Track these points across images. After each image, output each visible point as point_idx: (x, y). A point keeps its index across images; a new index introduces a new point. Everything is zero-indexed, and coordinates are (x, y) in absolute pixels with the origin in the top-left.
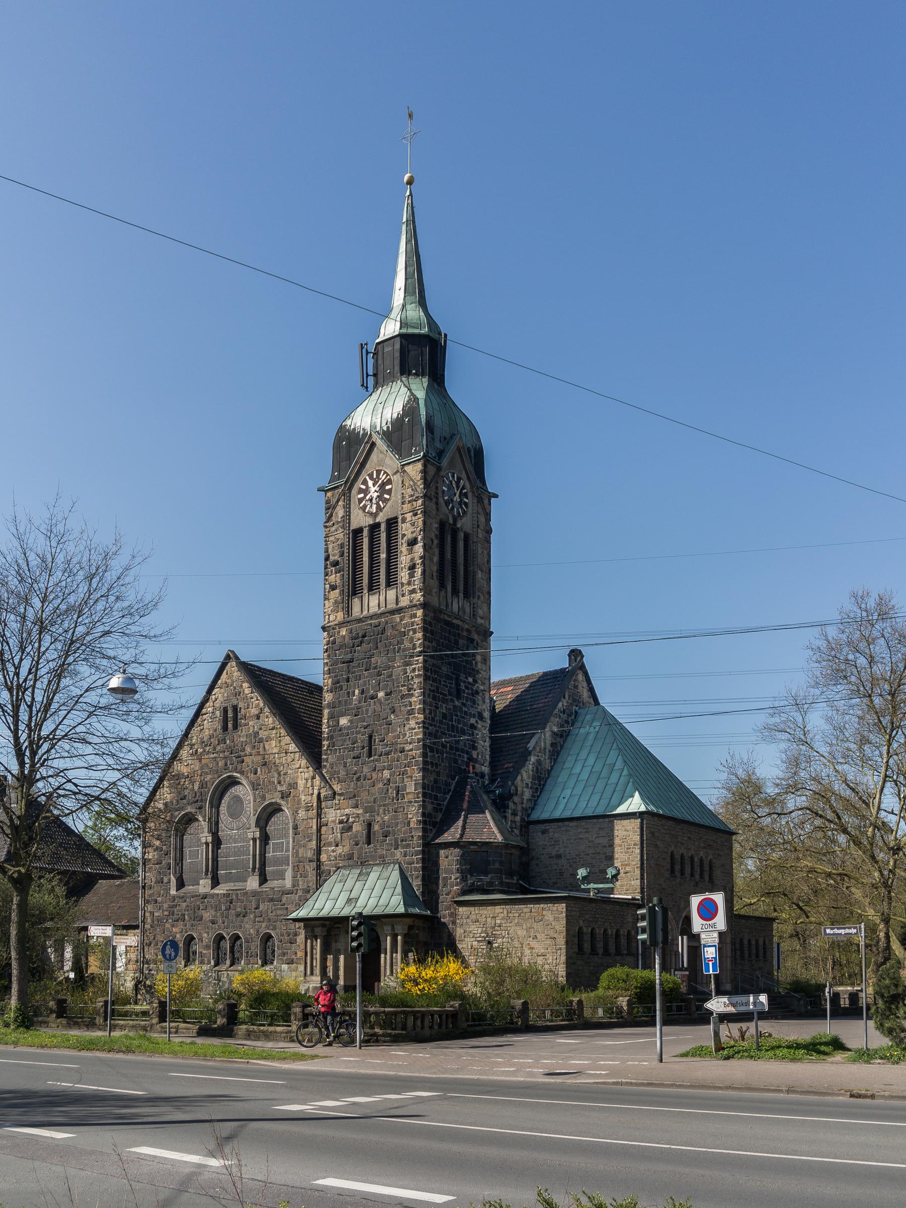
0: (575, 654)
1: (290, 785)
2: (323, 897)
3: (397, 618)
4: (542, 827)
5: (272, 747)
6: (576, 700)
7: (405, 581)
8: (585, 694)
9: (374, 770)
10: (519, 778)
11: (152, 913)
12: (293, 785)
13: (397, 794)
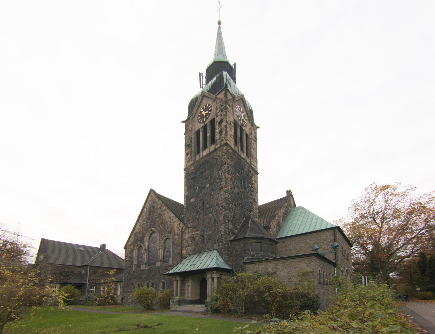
0: (289, 193)
1: (171, 228)
2: (181, 265)
3: (215, 154)
4: (282, 240)
5: (166, 217)
6: (290, 205)
7: (217, 138)
8: (293, 205)
9: (205, 215)
10: (272, 222)
11: (127, 277)
12: (173, 228)
13: (215, 222)
